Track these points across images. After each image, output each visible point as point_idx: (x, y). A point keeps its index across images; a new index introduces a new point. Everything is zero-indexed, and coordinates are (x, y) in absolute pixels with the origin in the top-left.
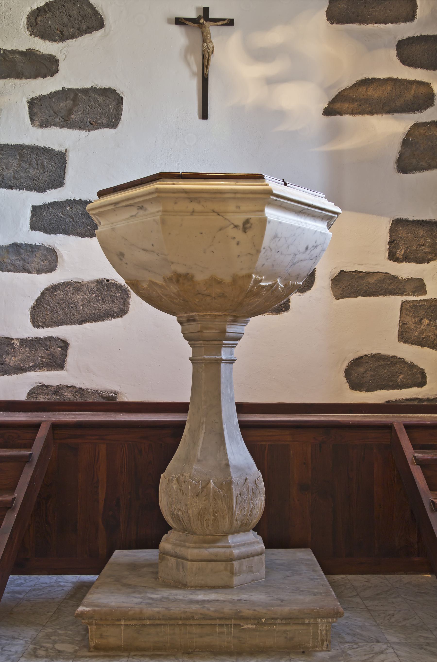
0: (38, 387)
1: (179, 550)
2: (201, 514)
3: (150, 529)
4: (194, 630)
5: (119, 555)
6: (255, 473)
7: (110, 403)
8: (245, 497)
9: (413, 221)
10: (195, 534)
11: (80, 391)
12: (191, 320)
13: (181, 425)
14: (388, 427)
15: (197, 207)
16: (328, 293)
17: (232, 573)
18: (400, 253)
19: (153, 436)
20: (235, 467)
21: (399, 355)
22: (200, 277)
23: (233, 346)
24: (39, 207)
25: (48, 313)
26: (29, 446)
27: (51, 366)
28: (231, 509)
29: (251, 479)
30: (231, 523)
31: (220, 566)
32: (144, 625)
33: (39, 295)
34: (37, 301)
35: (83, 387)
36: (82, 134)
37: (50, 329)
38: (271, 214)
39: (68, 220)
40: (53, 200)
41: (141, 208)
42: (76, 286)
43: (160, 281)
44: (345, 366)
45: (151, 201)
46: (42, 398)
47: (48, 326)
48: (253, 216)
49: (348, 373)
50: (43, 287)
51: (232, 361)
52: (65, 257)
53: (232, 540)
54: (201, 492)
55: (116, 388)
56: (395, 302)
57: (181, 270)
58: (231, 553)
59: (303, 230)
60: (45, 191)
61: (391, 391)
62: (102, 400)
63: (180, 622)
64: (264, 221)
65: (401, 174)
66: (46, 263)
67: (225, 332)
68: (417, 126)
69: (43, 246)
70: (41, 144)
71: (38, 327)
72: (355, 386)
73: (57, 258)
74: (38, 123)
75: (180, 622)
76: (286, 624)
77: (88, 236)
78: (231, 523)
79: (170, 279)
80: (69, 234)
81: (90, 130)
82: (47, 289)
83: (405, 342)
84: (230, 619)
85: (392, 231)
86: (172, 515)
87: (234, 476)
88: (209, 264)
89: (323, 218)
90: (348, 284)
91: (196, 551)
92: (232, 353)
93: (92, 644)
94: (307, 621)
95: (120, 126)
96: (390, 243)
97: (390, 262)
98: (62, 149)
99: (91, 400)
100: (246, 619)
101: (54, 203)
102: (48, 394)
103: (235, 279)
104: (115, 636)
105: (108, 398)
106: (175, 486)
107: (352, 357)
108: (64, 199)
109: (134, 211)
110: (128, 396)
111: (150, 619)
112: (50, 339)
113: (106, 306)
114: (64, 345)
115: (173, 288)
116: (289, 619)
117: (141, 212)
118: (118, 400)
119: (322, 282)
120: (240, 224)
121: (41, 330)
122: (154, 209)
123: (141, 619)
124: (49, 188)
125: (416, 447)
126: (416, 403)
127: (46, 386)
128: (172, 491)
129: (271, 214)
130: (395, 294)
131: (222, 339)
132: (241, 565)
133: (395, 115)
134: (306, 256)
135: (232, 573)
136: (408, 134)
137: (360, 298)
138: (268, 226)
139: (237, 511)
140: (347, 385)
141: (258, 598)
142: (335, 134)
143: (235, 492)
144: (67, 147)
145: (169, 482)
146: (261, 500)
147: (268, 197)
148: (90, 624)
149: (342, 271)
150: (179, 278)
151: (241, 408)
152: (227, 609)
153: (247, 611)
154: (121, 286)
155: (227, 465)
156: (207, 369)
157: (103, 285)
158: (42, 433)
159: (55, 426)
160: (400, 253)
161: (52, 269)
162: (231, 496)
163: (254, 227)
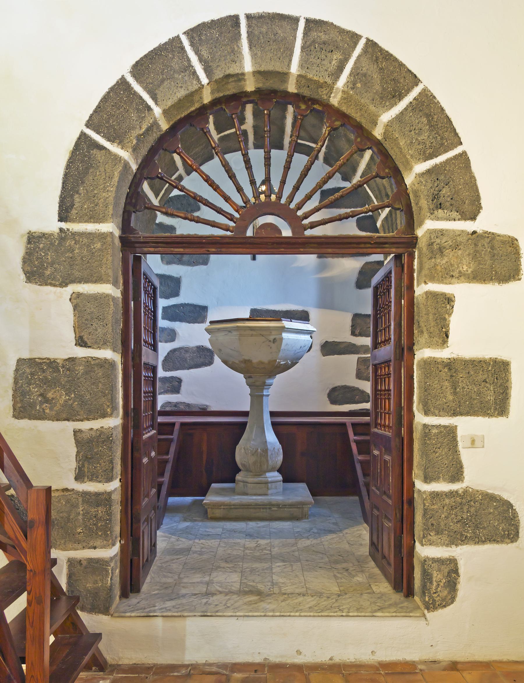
0: (166, 403)
1: (245, 479)
2: (255, 463)
3: (229, 472)
4: (252, 510)
5: (214, 485)
6: (278, 446)
7: (204, 412)
8: (274, 456)
9: (364, 315)
10: (251, 472)
11: (188, 405)
12: (250, 377)
13: (244, 424)
14: (344, 425)
15: (254, 333)
16: (319, 353)
17: (268, 489)
18: (357, 332)
19: (234, 428)
20: (269, 442)
21: (356, 386)
22: (255, 361)
23: (268, 389)
24: (166, 307)
25: (171, 363)
26: (172, 434)
27: (173, 392)
28: (267, 461)
29: (276, 448)
30: (268, 467)
31: (263, 485)
32: (231, 508)
33: (166, 354)
34: (165, 357)
35: (190, 403)
36: (189, 268)
37: (172, 372)
38: (285, 335)
39: (182, 314)
40: (173, 304)
41: (230, 332)
42: (186, 350)
43: (237, 362)
44: (328, 391)
45: (234, 330)
46: (168, 409)
47: (171, 371)
48: (277, 337)
49: (330, 395)
50: (169, 350)
51: (268, 395)
52: (180, 334)
53: (268, 474)
54: (255, 453)
55: (208, 404)
56: (354, 358)
57: (247, 358)
58: (268, 480)
59: (299, 340)
60: (169, 298)
61: (352, 405)
62: (199, 410)
63: (246, 507)
64: (281, 339)
65: (358, 290)
66: (170, 337)
67: (265, 383)
68: (367, 263)
69: (168, 328)
70: (167, 273)
71: (166, 371)
72: (333, 402)
73: (176, 334)
74: (165, 262)
75: (246, 507)
76: (290, 508)
77: (192, 323)
78: (268, 467)
79: (242, 362)
80: (182, 322)
81: (193, 266)
82: (171, 351)
83: (359, 379)
84: (267, 505)
85: (353, 320)
86: (242, 464)
87: (269, 446)
88: (259, 355)
89: (308, 334)
90: (330, 348)
91: (252, 479)
92: (268, 392)
93: (209, 517)
94: (299, 506)
95: (209, 264)
96: (352, 326)
97: (352, 337)
98: (178, 276)
99: (194, 410)
100: (273, 505)
101: (174, 305)
102: (171, 407)
103: (269, 362)
104: (218, 513)
105: (203, 409)
106: (243, 451)
107: (331, 387)
108: (180, 303)
109: (227, 333)
110: (214, 408)
111: (234, 506)
112: (172, 377)
113: (202, 360)
114: (179, 381)
115: (243, 365)
116: (292, 506)
117: (230, 334)
118: (208, 410)
119: (316, 348)
120: (272, 340)
121: (167, 372)
122: (235, 333)
123: (230, 506)
124: (171, 297)
125: (355, 434)
126: (365, 411)
127: (170, 402)
128: (240, 455)
129: (285, 335)
130: (354, 354)
131: (264, 386)
132: (272, 485)
133: (356, 258)
134: (301, 350)
135: (268, 489)
136: (362, 268)
137: (336, 356)
138: (283, 341)
139: (270, 462)
140: (329, 402)
141: (279, 498)
142: (322, 268)
143: (269, 454)
144: (181, 275)
145: (241, 449)
146: (281, 458)
147: (283, 329)
148: (209, 508)
149: (326, 342)
150: (246, 361)
151: (273, 414)
152: (266, 501)
153: (274, 502)
154: (210, 349)
155: (266, 442)
156: (257, 398)
157: (201, 349)
158: (177, 427)
159: (183, 424)
160: (357, 332)
161: (173, 340)
162: (268, 455)
163: (277, 341)
